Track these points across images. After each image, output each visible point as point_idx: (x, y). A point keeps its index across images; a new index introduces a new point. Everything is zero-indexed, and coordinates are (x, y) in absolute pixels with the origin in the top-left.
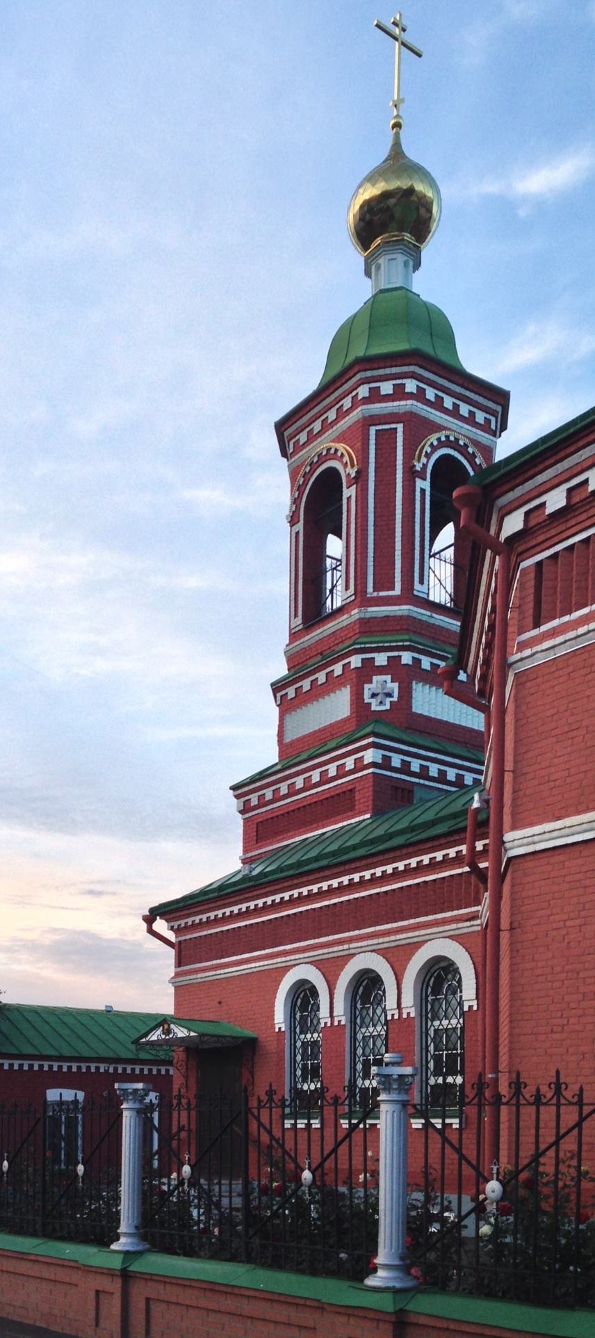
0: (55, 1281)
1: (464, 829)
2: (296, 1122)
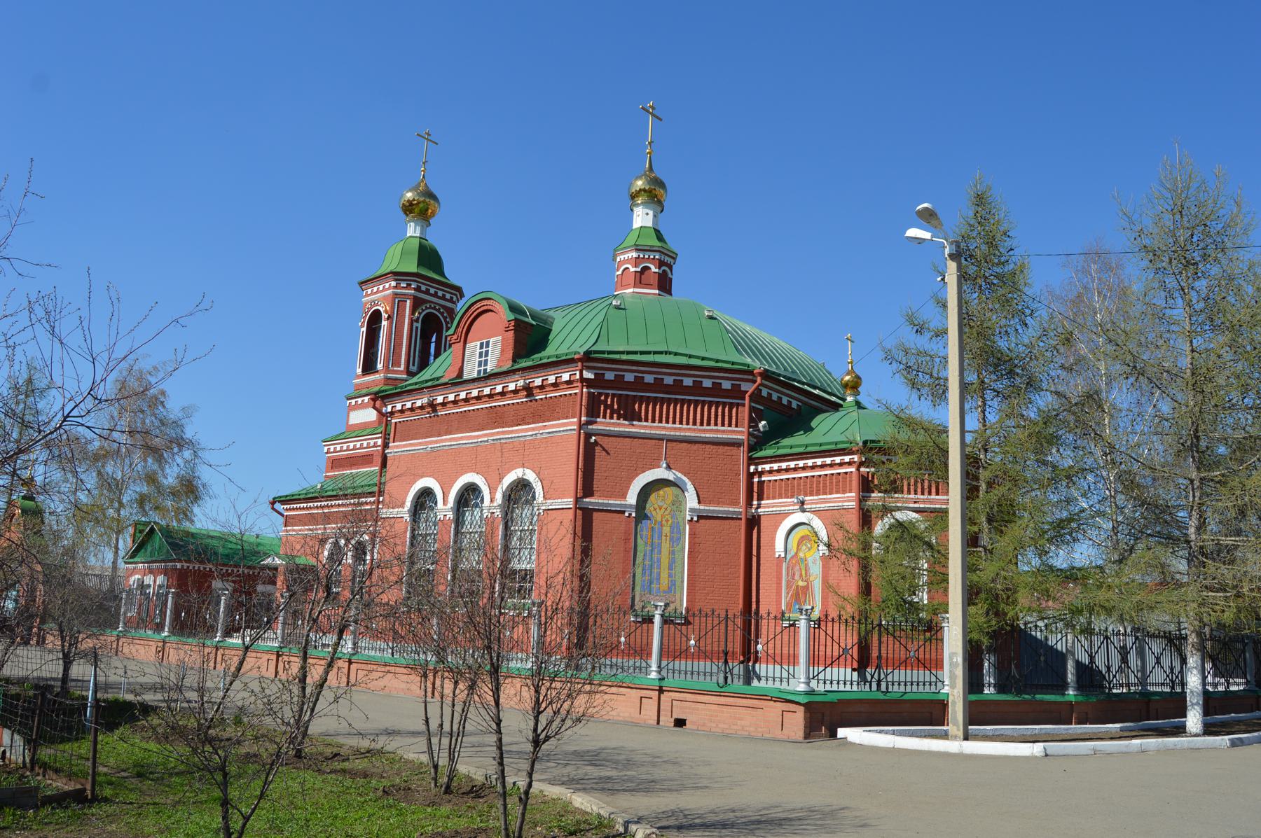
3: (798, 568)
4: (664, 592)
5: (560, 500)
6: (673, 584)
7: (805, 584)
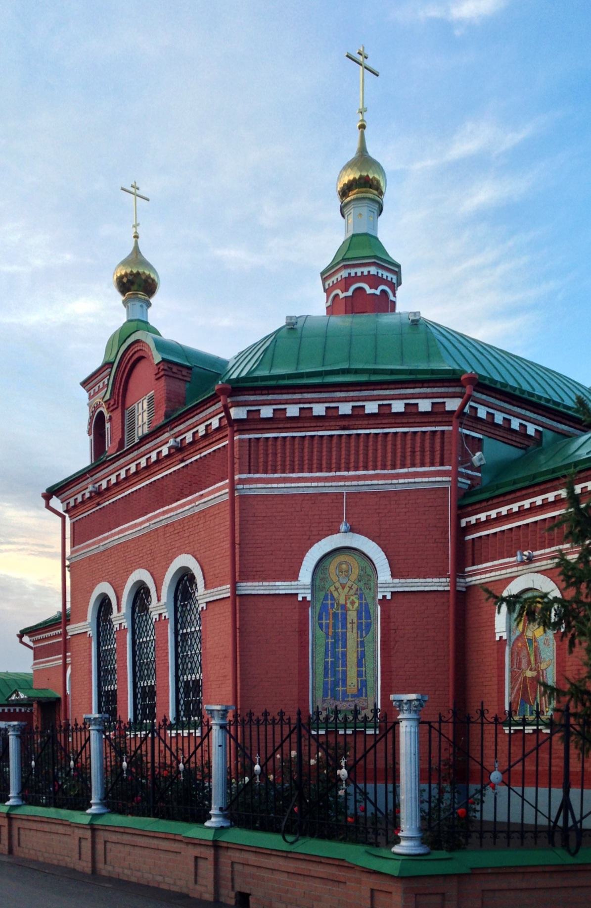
0: (37, 830)
1: (61, 622)
2: (524, 728)
3: (524, 653)
4: (353, 696)
5: (219, 588)
6: (364, 684)
7: (534, 674)
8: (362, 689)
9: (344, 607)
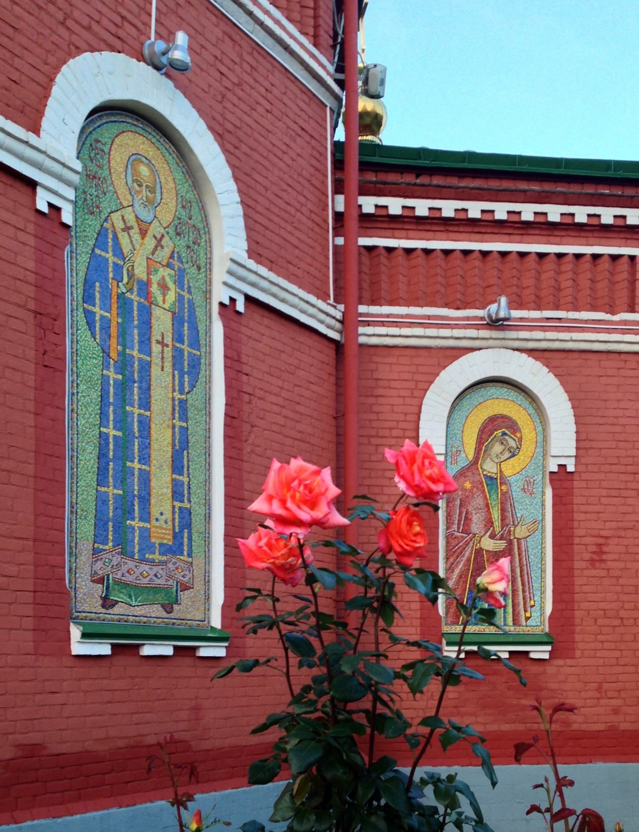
3: (479, 501)
4: (166, 550)
6: (185, 519)
8: (181, 531)
9: (144, 288)
